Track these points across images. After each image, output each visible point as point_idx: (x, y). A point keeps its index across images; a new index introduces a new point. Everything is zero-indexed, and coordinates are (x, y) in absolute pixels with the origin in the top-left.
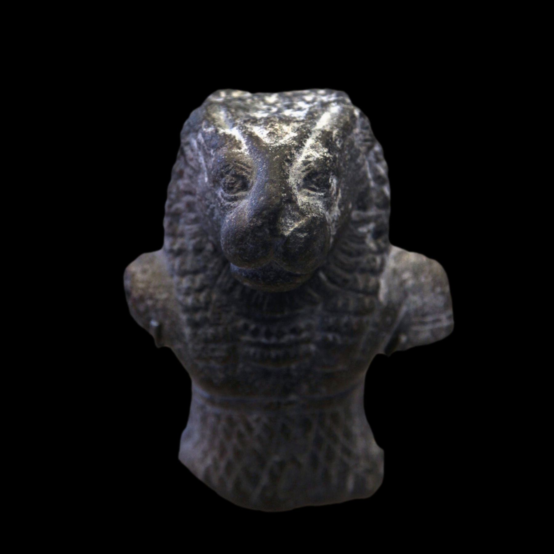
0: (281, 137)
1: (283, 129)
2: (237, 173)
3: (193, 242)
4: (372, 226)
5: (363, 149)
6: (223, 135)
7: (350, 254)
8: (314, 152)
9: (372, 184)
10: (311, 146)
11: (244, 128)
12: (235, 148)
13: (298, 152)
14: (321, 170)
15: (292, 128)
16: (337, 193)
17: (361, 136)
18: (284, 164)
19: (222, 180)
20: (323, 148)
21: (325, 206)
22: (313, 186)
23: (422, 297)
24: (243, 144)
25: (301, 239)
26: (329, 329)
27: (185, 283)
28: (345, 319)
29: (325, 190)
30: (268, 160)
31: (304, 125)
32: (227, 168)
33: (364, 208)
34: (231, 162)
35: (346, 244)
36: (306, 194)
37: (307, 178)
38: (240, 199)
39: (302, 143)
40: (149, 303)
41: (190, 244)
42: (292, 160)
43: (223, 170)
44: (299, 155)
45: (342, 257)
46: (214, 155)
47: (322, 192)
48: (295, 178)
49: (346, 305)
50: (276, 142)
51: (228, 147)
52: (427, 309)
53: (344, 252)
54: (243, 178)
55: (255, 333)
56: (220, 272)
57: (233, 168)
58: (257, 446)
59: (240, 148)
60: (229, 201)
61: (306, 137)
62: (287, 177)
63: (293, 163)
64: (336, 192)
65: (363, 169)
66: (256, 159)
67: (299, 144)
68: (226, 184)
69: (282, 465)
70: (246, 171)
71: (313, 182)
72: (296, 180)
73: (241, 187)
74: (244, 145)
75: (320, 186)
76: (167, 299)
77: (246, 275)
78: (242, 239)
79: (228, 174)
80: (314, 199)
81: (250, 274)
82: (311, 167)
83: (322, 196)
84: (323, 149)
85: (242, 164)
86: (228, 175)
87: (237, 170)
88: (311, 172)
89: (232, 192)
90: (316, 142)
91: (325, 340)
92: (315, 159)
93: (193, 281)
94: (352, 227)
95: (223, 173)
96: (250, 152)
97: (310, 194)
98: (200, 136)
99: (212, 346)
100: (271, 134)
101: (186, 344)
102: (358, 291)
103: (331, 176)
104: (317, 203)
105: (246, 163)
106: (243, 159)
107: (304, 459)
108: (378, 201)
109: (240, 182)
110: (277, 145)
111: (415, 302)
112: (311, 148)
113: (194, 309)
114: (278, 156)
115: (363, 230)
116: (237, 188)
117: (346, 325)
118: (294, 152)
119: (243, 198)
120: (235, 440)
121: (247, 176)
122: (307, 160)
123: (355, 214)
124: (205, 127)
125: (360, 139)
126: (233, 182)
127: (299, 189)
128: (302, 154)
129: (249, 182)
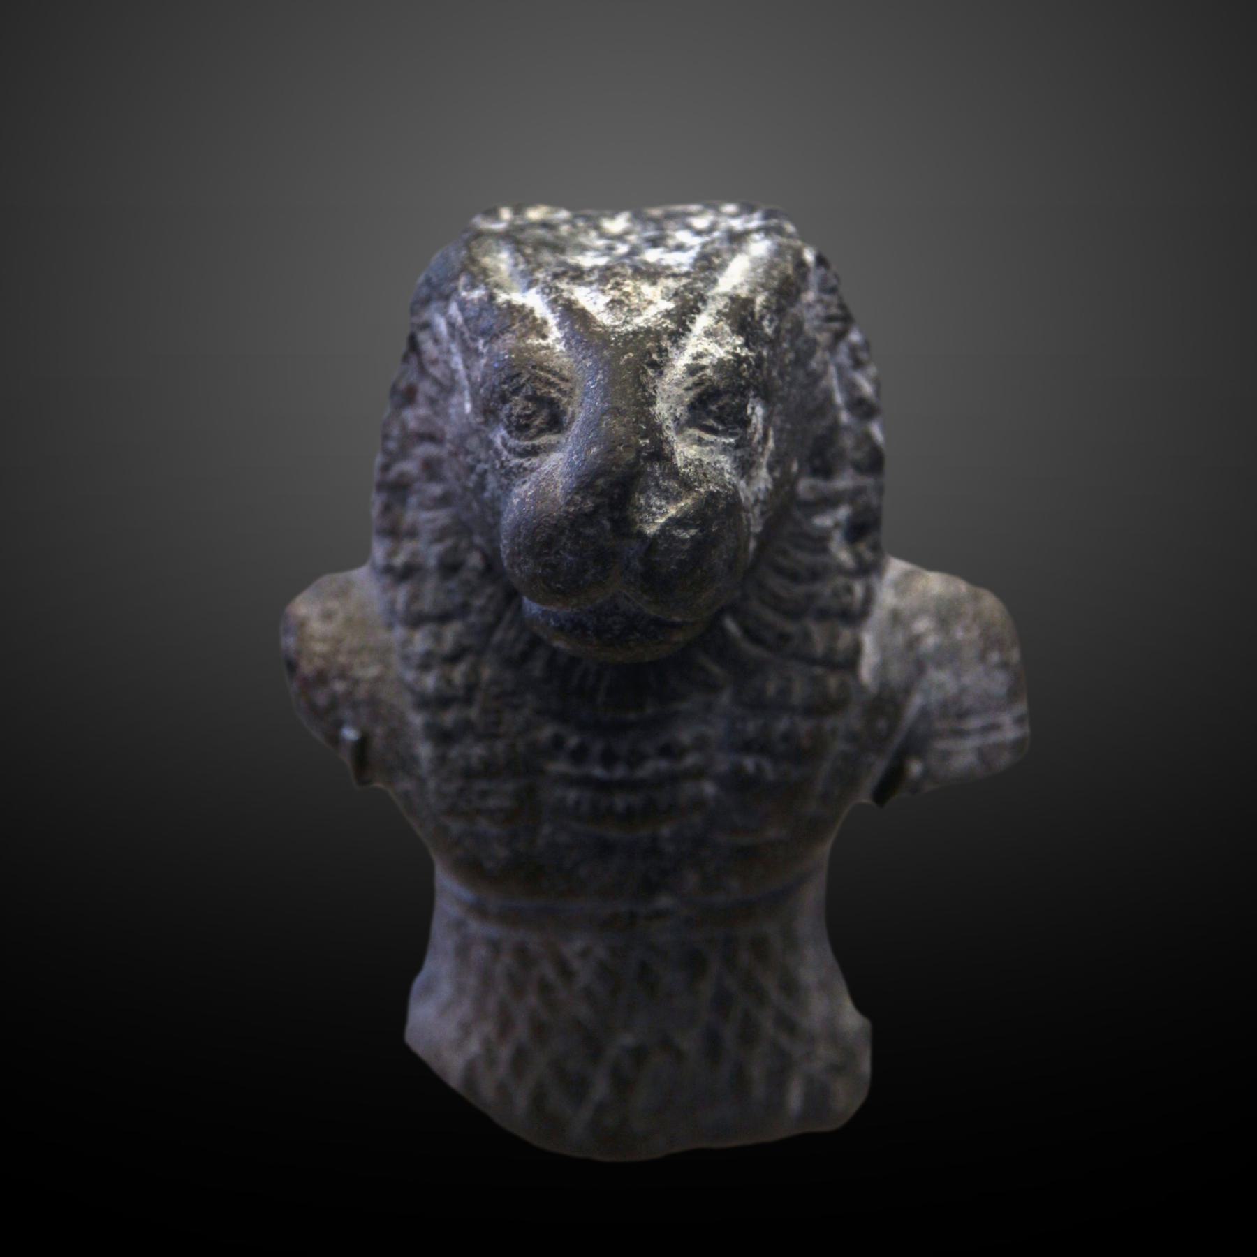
0: (639, 312)
1: (642, 293)
2: (539, 393)
3: (437, 549)
4: (843, 513)
5: (823, 338)
6: (505, 306)
7: (795, 577)
8: (711, 344)
9: (844, 417)
10: (705, 332)
11: (554, 290)
12: (532, 336)
13: (675, 344)
14: (729, 386)
15: (662, 291)
16: (765, 437)
17: (819, 309)
18: (645, 372)
19: (504, 408)
20: (733, 335)
21: (738, 467)
22: (711, 422)
23: (958, 675)
24: (552, 326)
25: (683, 541)
26: (747, 747)
27: (421, 642)
28: (782, 725)
29: (738, 430)
30: (608, 362)
31: (689, 284)
32: (515, 381)
33: (826, 472)
34: (523, 367)
35: (784, 553)
36: (694, 439)
37: (697, 404)
38: (545, 452)
39: (686, 325)
40: (339, 687)
41: (432, 554)
42: (662, 362)
43: (506, 387)
44: (678, 352)
45: (776, 584)
46: (485, 351)
47: (732, 435)
48: (669, 405)
49: (784, 692)
50: (626, 322)
51: (518, 333)
52: (968, 702)
53: (780, 571)
54: (552, 403)
55: (579, 755)
56: (499, 618)
57: (529, 382)
58: (583, 1011)
59: (544, 337)
60: (521, 455)
61: (695, 311)
62: (651, 401)
63: (666, 371)
64: (762, 435)
65: (824, 383)
66: (580, 362)
67: (679, 326)
68: (513, 417)
69: (639, 1055)
70: (558, 388)
71: (709, 413)
72: (671, 407)
73: (548, 424)
74: (555, 329)
75: (726, 422)
76: (378, 680)
77: (557, 625)
78: (549, 543)
79: (518, 395)
80: (712, 451)
81: (566, 621)
82: (705, 380)
83: (730, 444)
84: (734, 337)
85: (549, 371)
86: (517, 398)
87: (538, 385)
88: (706, 390)
89: (526, 436)
90: (717, 322)
91: (737, 771)
92: (715, 362)
93: (438, 638)
94: (798, 514)
95: (507, 393)
96: (567, 346)
97: (703, 439)
98: (453, 309)
99: (481, 785)
100: (614, 304)
101: (422, 781)
102: (812, 661)
103: (751, 400)
104: (718, 461)
105: (558, 369)
106: (552, 361)
107: (689, 1042)
108: (858, 455)
109: (545, 413)
110: (630, 328)
111: (941, 686)
112: (705, 337)
113: (441, 701)
114: (631, 355)
115: (824, 521)
116: (537, 426)
117: (786, 737)
118: (666, 344)
119: (550, 448)
120: (532, 999)
121: (560, 400)
122: (697, 364)
123: (805, 486)
124: (465, 288)
125: (817, 316)
126: (528, 412)
127: (680, 430)
128: (684, 350)
129: (564, 412)
